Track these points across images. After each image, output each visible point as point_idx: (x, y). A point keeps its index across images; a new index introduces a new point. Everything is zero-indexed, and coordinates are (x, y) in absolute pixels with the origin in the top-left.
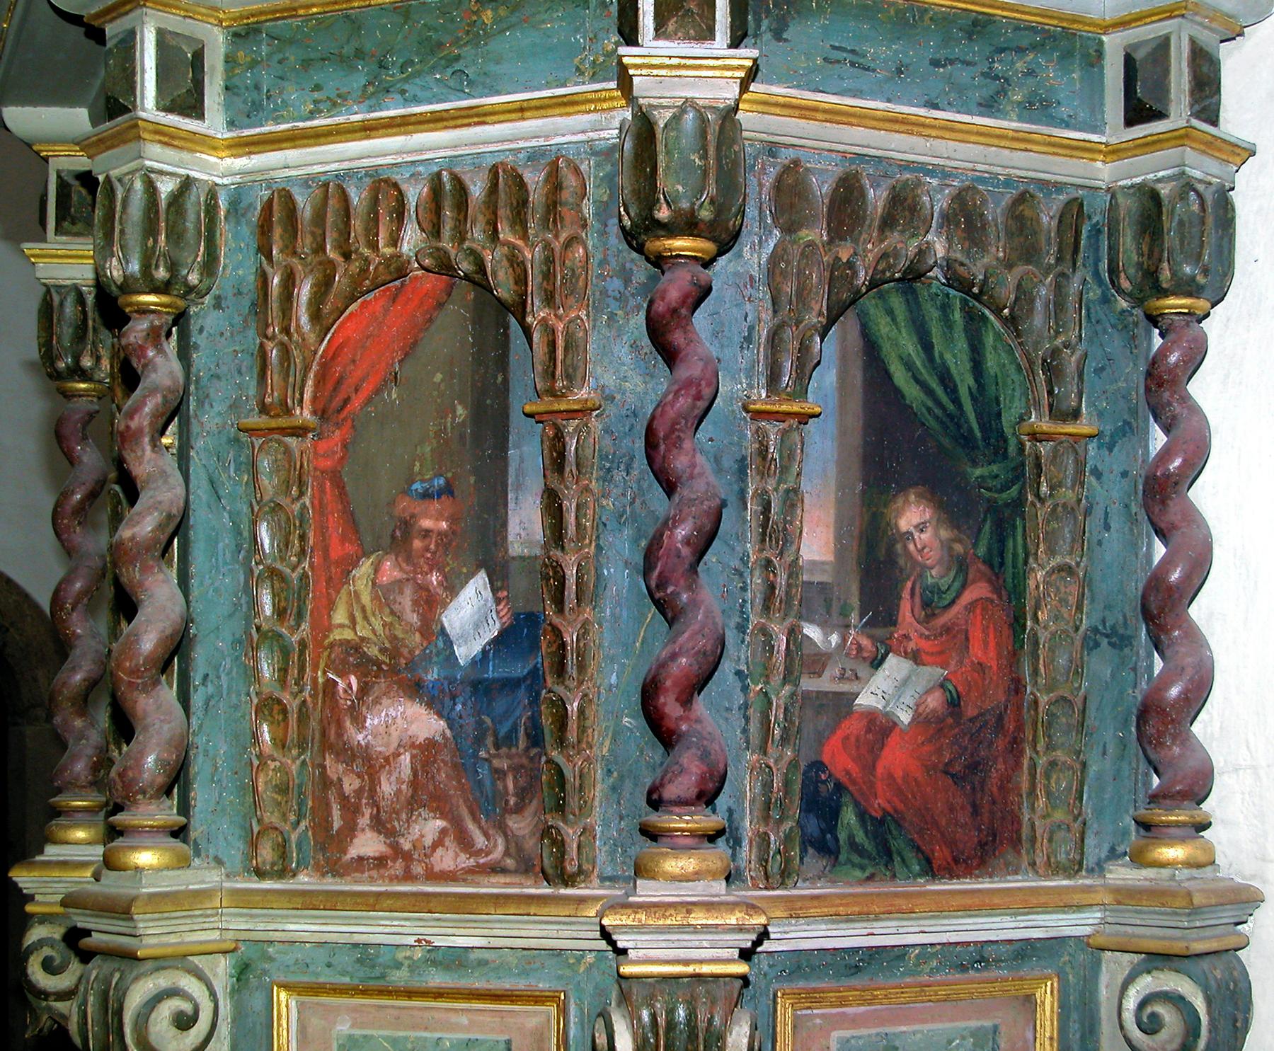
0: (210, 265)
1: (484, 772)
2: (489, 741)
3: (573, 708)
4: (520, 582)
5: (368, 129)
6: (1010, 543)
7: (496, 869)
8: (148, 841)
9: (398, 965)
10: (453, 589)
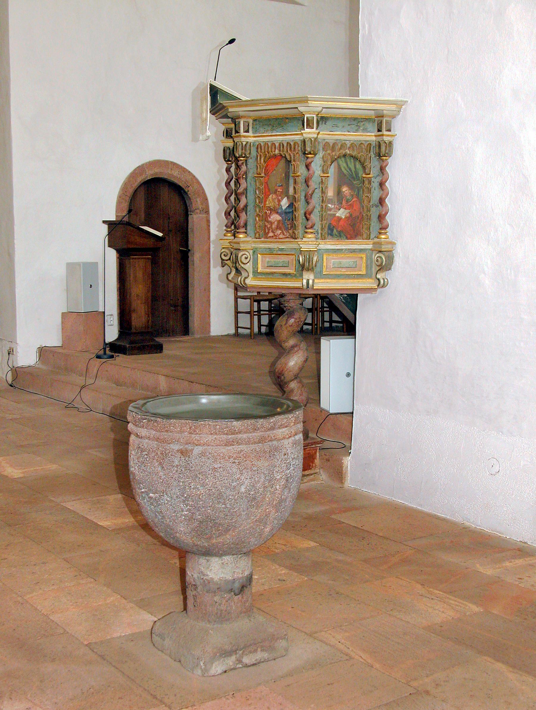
0: (250, 153)
1: (286, 224)
2: (287, 220)
3: (297, 216)
4: (291, 198)
5: (271, 136)
6: (360, 193)
7: (287, 238)
8: (242, 234)
9: (275, 251)
10: (282, 199)
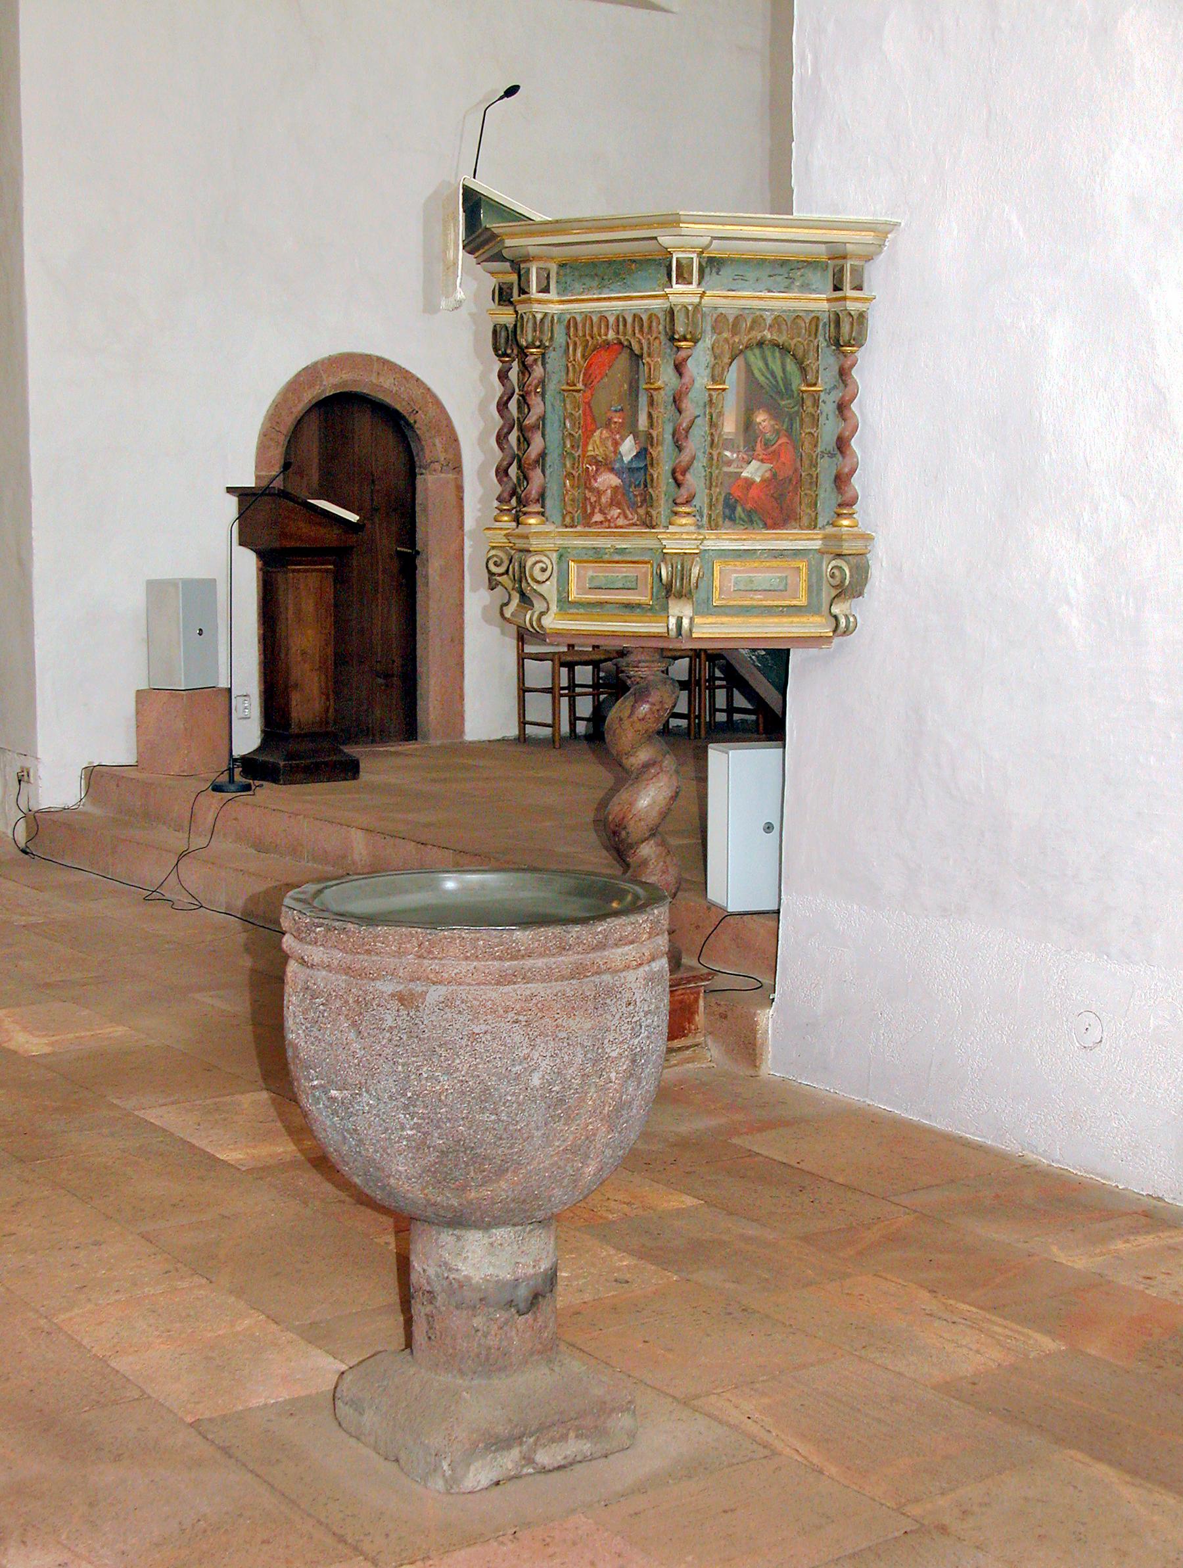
0: (551, 339)
1: (631, 495)
2: (633, 486)
3: (655, 476)
4: (642, 438)
5: (598, 300)
6: (794, 425)
7: (634, 525)
8: (533, 516)
9: (606, 554)
10: (623, 439)
